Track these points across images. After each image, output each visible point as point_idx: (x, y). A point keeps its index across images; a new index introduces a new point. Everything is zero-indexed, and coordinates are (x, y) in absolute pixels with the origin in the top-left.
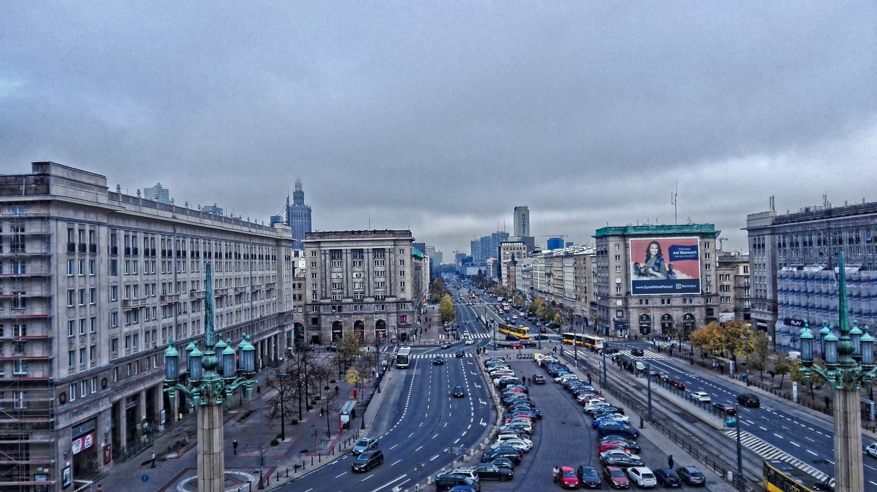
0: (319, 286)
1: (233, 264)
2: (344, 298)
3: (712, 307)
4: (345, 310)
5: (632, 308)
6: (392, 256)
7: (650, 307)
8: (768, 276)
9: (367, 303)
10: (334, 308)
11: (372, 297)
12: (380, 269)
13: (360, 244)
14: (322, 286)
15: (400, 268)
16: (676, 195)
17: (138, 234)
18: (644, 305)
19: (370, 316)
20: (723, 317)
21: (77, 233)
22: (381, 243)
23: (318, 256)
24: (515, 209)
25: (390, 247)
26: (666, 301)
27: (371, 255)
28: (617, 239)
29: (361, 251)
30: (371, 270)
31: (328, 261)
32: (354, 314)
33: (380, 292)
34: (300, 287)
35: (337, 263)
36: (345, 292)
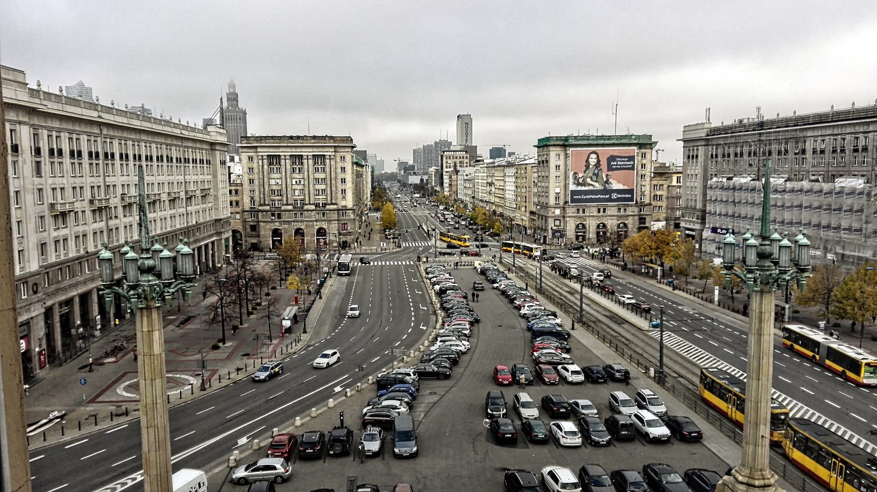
0: (257, 193)
1: (165, 168)
4: (285, 217)
5: (569, 217)
6: (333, 162)
8: (699, 186)
9: (308, 211)
10: (273, 215)
11: (290, 205)
13: (298, 150)
14: (260, 192)
15: (341, 176)
18: (581, 214)
19: (311, 223)
22: (321, 150)
23: (255, 161)
24: (458, 117)
25: (331, 154)
26: (602, 210)
27: (311, 161)
28: (558, 149)
29: (301, 157)
30: (311, 176)
31: (266, 167)
32: (294, 221)
33: (321, 199)
35: (275, 169)
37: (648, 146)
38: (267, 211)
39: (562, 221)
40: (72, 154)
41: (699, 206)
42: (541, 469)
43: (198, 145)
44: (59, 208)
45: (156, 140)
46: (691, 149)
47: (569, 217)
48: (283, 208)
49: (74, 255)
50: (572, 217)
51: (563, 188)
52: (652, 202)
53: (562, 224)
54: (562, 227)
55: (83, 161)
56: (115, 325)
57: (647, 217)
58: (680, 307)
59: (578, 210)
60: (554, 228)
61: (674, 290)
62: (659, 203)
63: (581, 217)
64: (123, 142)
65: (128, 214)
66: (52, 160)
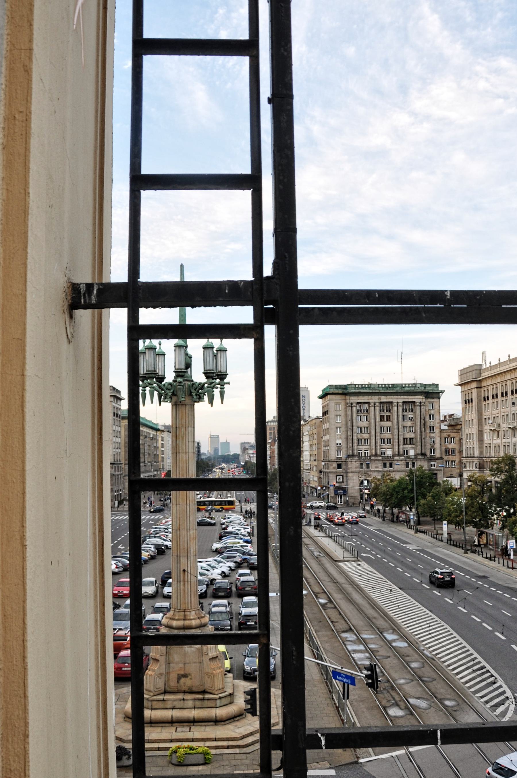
5: (352, 472)
7: (371, 471)
8: (475, 432)
16: (402, 353)
26: (388, 465)
28: (338, 397)
37: (435, 395)
39: (345, 478)
41: (476, 454)
42: (285, 755)
43: (214, 496)
46: (470, 392)
47: (352, 472)
50: (356, 472)
51: (344, 440)
52: (444, 456)
53: (345, 480)
54: (345, 483)
57: (438, 472)
58: (408, 546)
59: (362, 464)
60: (337, 485)
61: (416, 533)
62: (451, 458)
63: (366, 473)
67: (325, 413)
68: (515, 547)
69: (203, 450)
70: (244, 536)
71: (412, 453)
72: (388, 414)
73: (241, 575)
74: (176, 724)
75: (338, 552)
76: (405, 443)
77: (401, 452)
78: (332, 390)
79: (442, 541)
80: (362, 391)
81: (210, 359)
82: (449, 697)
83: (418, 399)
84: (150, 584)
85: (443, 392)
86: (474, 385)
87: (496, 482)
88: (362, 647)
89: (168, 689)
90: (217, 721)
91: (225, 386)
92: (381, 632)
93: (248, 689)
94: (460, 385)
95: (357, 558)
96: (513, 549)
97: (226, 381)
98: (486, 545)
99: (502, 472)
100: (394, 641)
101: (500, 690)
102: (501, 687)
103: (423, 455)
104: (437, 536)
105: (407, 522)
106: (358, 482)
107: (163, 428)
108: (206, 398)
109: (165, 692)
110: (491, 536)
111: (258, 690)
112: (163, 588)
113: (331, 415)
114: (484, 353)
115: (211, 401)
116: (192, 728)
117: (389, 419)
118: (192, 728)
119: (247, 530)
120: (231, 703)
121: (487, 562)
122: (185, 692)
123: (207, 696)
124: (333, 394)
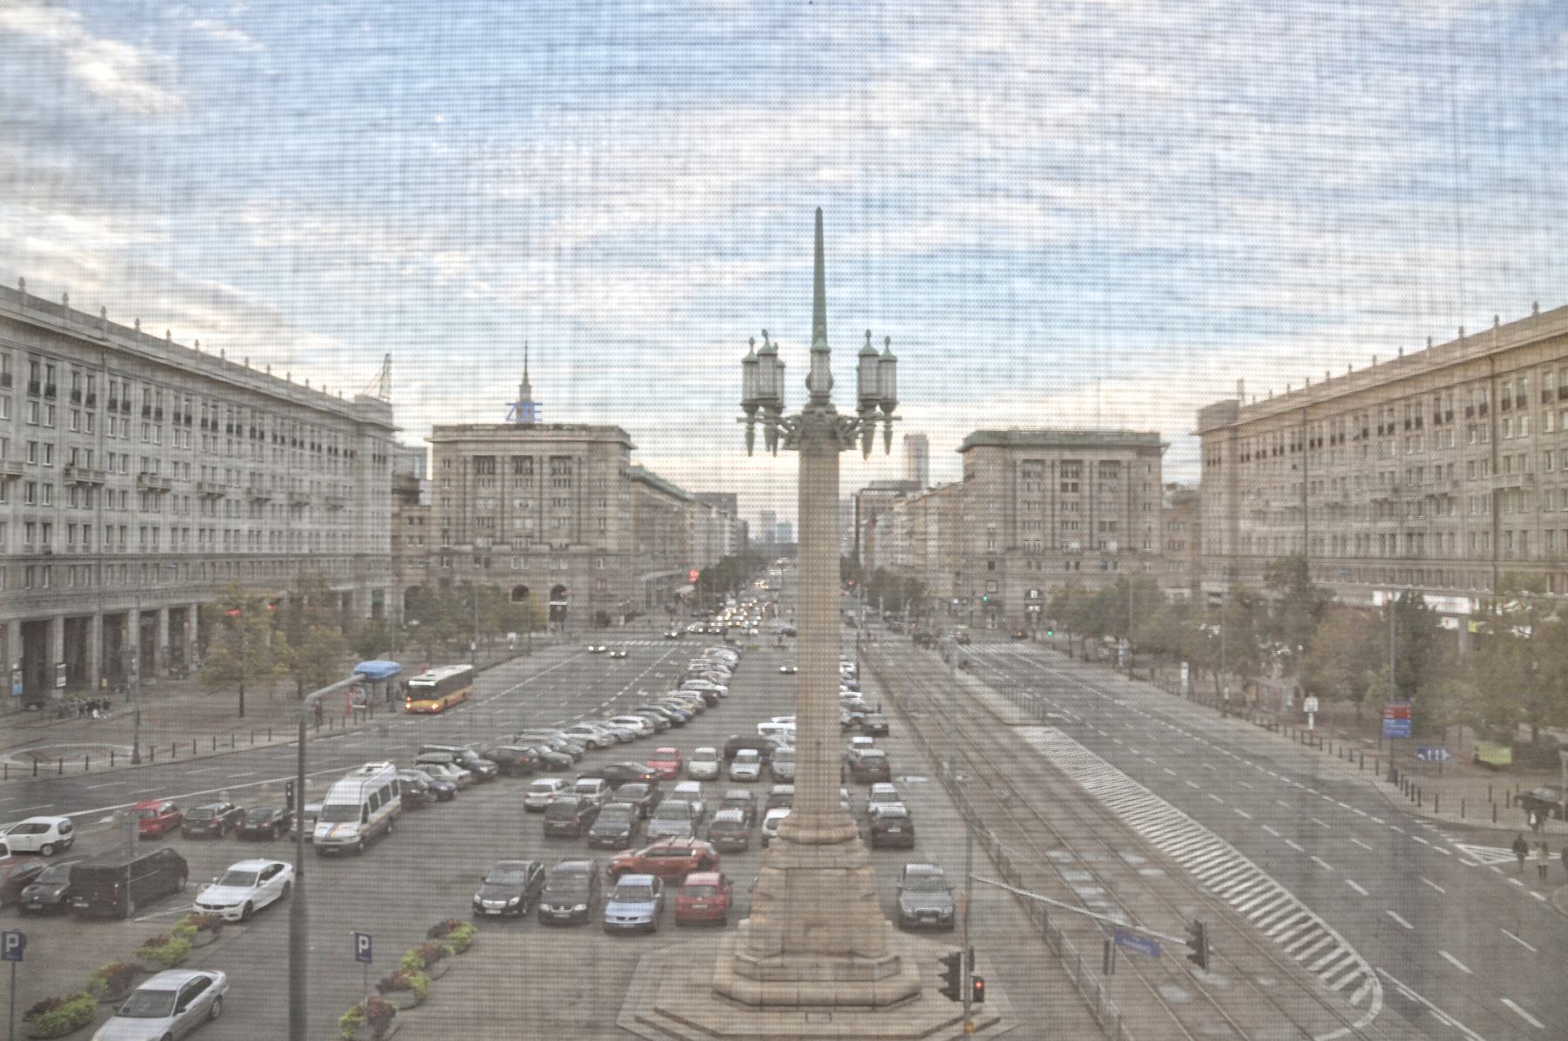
1: (307, 458)
2: (494, 543)
3: (95, 507)
4: (498, 566)
10: (477, 560)
12: (564, 493)
17: (59, 365)
20: (760, 884)
21: (120, 386)
34: (421, 524)
36: (498, 534)
38: (466, 554)
40: (204, 423)
44: (207, 489)
45: (231, 397)
48: (495, 548)
49: (267, 551)
55: (57, 403)
56: (101, 688)
64: (153, 389)
65: (256, 514)
66: (77, 408)
67: (969, 477)
68: (1316, 709)
69: (751, 536)
70: (846, 679)
71: (1113, 546)
72: (1075, 481)
73: (859, 746)
74: (805, 1008)
75: (1011, 712)
76: (1102, 529)
77: (1096, 545)
78: (980, 441)
79: (1179, 694)
80: (1034, 442)
81: (871, 375)
82: (1261, 970)
83: (1126, 456)
84: (707, 757)
85: (1167, 445)
86: (1226, 435)
87: (1276, 601)
88: (1086, 876)
89: (787, 947)
90: (874, 1005)
91: (894, 423)
92: (1113, 850)
93: (945, 955)
94: (1201, 435)
95: (1043, 721)
96: (1314, 713)
97: (894, 414)
98: (1256, 704)
99: (1285, 583)
100: (1142, 866)
101: (1348, 961)
102: (1346, 954)
103: (1132, 549)
104: (1170, 687)
105: (1113, 660)
106: (1022, 595)
107: (693, 497)
108: (858, 442)
109: (783, 952)
110: (1265, 690)
111: (963, 956)
112: (730, 763)
113: (981, 478)
114: (1241, 381)
115: (867, 449)
116: (834, 1015)
117: (1075, 487)
118: (834, 1015)
119: (850, 669)
120: (898, 972)
121: (1264, 733)
122: (817, 952)
123: (858, 961)
124: (983, 445)
